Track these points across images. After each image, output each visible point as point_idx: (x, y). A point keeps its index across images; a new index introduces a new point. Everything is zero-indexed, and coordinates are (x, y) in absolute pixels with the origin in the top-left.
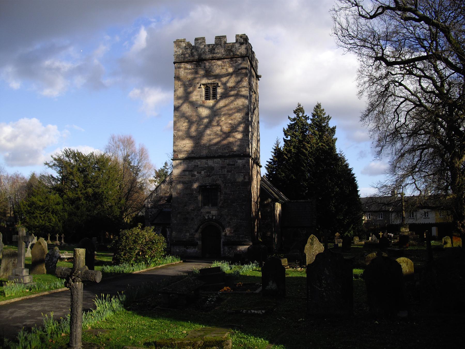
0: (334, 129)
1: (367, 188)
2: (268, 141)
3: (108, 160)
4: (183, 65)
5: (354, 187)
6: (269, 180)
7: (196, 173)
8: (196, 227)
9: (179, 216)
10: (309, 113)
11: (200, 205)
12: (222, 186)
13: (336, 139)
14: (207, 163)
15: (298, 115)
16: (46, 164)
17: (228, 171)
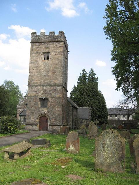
0: (97, 78)
1: (109, 105)
2: (72, 83)
4: (34, 44)
5: (104, 103)
6: (71, 99)
8: (37, 117)
13: (98, 83)
14: (43, 88)
15: (83, 72)
17: (52, 92)
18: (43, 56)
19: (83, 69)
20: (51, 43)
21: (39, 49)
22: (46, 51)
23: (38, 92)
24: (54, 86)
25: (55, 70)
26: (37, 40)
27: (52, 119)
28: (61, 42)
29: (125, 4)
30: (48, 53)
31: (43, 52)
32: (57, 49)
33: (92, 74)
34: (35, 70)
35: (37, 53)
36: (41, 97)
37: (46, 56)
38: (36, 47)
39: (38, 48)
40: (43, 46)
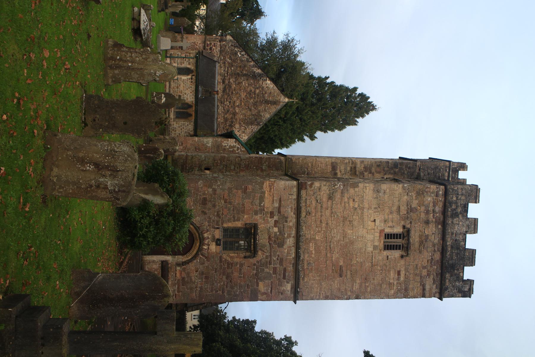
4: (441, 198)
18: (398, 230)
19: (496, 239)
20: (437, 256)
21: (423, 216)
22: (415, 238)
23: (276, 218)
24: (297, 272)
25: (349, 273)
26: (454, 207)
27: (184, 270)
28: (438, 290)
29: (225, 319)
30: (406, 248)
31: (412, 233)
32: (418, 279)
33: (356, 125)
34: (351, 205)
35: (411, 210)
36: (261, 226)
37: (399, 242)
38: (431, 205)
39: (427, 212)
40: (432, 231)
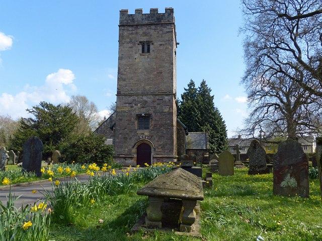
0: (213, 97)
3: (70, 110)
7: (134, 105)
8: (133, 144)
9: (120, 136)
10: (197, 85)
11: (136, 129)
12: (153, 114)
14: (142, 98)
16: (27, 110)
